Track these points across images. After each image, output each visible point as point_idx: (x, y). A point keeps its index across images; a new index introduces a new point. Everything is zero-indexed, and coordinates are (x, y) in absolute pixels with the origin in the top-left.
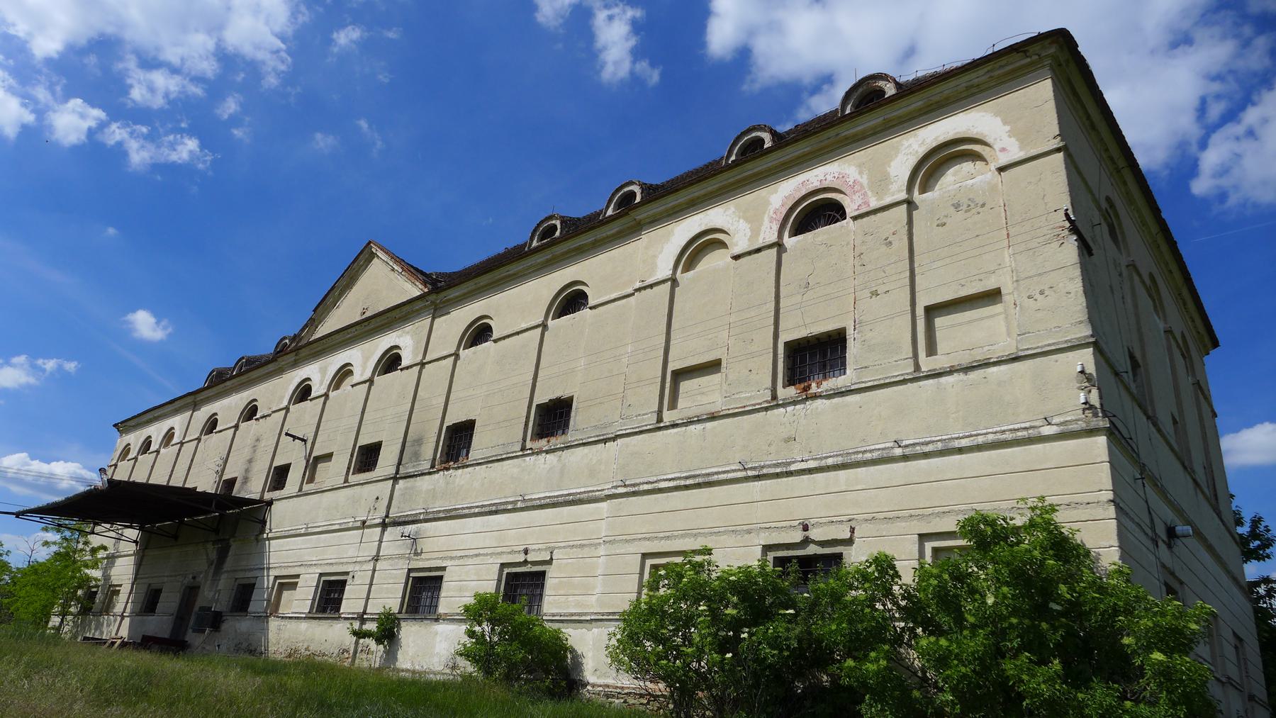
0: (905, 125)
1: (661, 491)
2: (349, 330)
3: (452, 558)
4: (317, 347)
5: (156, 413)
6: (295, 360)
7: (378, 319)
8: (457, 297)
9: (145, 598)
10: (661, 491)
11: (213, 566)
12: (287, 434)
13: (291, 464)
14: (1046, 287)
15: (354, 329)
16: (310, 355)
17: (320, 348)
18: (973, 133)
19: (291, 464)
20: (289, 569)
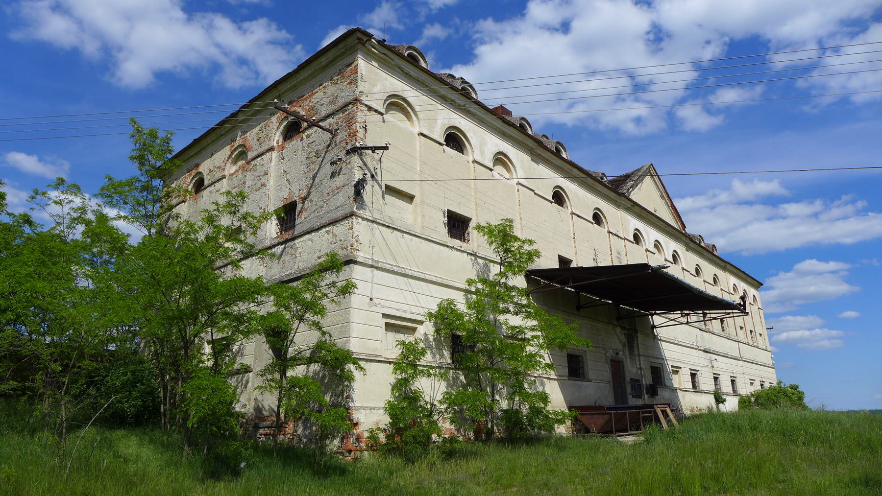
0: (496, 132)
1: (748, 362)
2: (660, 222)
3: (722, 371)
4: (644, 214)
5: (749, 280)
6: (629, 208)
7: (671, 229)
8: (691, 247)
9: (664, 376)
10: (748, 362)
11: (627, 348)
12: (743, 318)
13: (559, 255)
14: (477, 216)
15: (662, 223)
16: (637, 213)
17: (644, 216)
18: (511, 157)
19: (559, 255)
20: (676, 363)
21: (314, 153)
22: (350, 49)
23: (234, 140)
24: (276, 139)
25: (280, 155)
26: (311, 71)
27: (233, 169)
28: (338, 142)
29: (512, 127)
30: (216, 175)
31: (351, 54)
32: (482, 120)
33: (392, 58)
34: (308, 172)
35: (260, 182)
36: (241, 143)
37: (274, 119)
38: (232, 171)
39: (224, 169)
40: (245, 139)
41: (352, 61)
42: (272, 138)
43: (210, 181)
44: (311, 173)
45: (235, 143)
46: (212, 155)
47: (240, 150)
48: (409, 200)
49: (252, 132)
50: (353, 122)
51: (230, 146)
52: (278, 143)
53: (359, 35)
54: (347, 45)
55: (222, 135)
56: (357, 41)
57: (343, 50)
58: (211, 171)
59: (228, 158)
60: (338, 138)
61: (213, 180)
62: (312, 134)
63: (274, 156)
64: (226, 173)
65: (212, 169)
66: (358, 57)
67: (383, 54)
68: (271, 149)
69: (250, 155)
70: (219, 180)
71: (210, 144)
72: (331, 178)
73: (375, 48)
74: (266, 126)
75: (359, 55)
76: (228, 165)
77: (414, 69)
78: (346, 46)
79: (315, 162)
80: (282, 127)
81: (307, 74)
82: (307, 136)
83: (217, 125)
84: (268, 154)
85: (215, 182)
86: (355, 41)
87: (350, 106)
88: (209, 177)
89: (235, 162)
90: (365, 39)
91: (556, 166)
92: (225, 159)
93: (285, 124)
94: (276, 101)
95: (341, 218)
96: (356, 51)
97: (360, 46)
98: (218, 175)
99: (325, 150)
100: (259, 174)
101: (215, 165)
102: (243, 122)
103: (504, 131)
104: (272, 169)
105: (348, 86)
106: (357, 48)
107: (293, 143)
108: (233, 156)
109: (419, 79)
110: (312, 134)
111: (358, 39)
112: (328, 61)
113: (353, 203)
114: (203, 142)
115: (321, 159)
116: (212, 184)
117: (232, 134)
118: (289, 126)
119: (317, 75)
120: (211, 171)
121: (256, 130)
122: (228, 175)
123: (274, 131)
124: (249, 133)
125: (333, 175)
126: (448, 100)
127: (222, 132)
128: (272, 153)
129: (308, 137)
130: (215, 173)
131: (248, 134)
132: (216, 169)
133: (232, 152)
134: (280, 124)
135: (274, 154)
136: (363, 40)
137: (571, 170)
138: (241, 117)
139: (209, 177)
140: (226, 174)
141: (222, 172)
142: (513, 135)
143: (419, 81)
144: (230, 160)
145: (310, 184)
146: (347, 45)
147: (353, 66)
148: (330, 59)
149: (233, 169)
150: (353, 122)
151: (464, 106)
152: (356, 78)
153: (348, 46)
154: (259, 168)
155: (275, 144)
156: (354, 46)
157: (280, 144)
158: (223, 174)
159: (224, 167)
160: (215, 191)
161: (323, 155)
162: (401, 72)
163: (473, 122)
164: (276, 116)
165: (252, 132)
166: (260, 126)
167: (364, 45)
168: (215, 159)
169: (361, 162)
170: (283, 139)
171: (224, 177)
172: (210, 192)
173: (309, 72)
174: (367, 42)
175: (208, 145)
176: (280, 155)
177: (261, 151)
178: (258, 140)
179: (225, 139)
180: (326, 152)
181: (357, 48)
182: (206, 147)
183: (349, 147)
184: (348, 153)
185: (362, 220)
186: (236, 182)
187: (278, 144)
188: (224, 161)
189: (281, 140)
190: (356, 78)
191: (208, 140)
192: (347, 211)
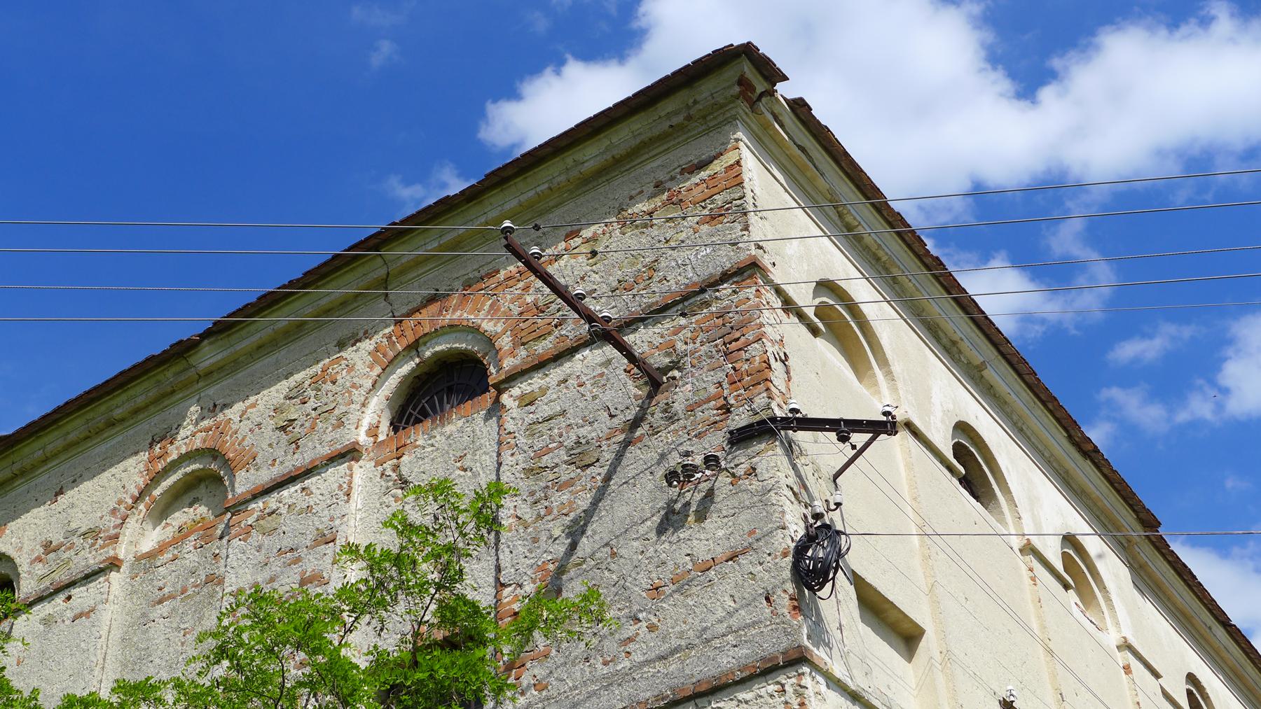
21: (562, 452)
22: (704, 117)
23: (167, 435)
24: (367, 420)
25: (389, 472)
26: (531, 193)
27: (151, 538)
28: (678, 407)
29: (1088, 462)
30: (76, 559)
31: (708, 131)
32: (1020, 425)
33: (820, 167)
34: (540, 517)
35: (296, 569)
36: (198, 444)
37: (360, 355)
38: (147, 545)
39: (116, 537)
40: (220, 430)
41: (713, 153)
42: (353, 418)
43: (47, 583)
44: (558, 523)
45: (170, 448)
46: (61, 492)
47: (189, 469)
48: (902, 646)
49: (254, 405)
50: (750, 336)
51: (144, 456)
52: (373, 431)
53: (747, 69)
54: (695, 102)
55: (111, 424)
56: (737, 89)
57: (676, 120)
58: (48, 547)
59: (137, 500)
60: (681, 396)
61: (62, 577)
62: (543, 391)
63: (357, 480)
64: (122, 550)
65: (57, 538)
66: (737, 140)
67: (799, 147)
68: (350, 453)
69: (243, 483)
70: (89, 577)
71: (55, 455)
72: (661, 530)
73: (782, 126)
74: (316, 381)
75: (740, 135)
76: (132, 523)
77: (872, 218)
78: (688, 107)
79: (570, 483)
80: (393, 381)
81: (531, 193)
82: (521, 397)
83: (291, 284)
84: (335, 474)
85: (72, 584)
86: (729, 87)
87: (726, 289)
88: (40, 569)
89: (161, 512)
90: (760, 87)
91: (1177, 608)
92: (120, 502)
93: (406, 369)
94: (507, 223)
95: (739, 675)
96: (731, 121)
97: (742, 107)
98: (91, 558)
99: (621, 437)
100: (287, 542)
101: (73, 526)
102: (208, 375)
103: (1067, 472)
104: (352, 523)
105: (705, 228)
106: (733, 112)
107: (449, 429)
108: (157, 492)
109: (880, 253)
110: (543, 391)
111: (743, 82)
112: (608, 156)
113: (793, 617)
114: (26, 450)
115: (604, 471)
116: (58, 591)
117: (156, 419)
118: (417, 377)
119: (556, 206)
120: (48, 547)
121: (275, 393)
122: (131, 557)
123: (358, 396)
124: (239, 407)
125: (671, 520)
126: (944, 340)
127: (118, 413)
128: (350, 469)
129: (528, 401)
130: (72, 552)
131: (233, 413)
132: (78, 541)
133: (155, 479)
134: (389, 367)
135: (362, 473)
136: (753, 89)
137: (1210, 628)
138: (208, 357)
139: (40, 569)
140: (121, 557)
141: (102, 547)
142: (1090, 488)
143: (878, 259)
144: (142, 507)
145: (553, 561)
146: (695, 102)
147: (717, 167)
148: (617, 152)
149: (151, 538)
150: (750, 336)
151: (981, 368)
152: (738, 202)
153: (699, 107)
154: (289, 523)
155: (362, 438)
156: (722, 106)
157: (381, 438)
158: (112, 553)
159: (113, 532)
160: (69, 614)
161: (608, 456)
162: (836, 218)
163: (1002, 423)
164: (367, 345)
165: (254, 405)
166: (292, 381)
167: (753, 104)
168: (72, 506)
169: (792, 473)
170: (391, 424)
171: (114, 564)
172: (47, 621)
173: (523, 198)
174: (764, 100)
175: (45, 461)
176: (389, 472)
177: (298, 464)
178: (283, 429)
179: (119, 438)
180: (627, 444)
181: (733, 112)
182: (34, 468)
183: (740, 419)
184: (741, 438)
185: (828, 687)
186: (171, 578)
187: (376, 436)
188: (114, 512)
189: (385, 427)
190: (738, 202)
191: (52, 440)
192: (773, 645)
